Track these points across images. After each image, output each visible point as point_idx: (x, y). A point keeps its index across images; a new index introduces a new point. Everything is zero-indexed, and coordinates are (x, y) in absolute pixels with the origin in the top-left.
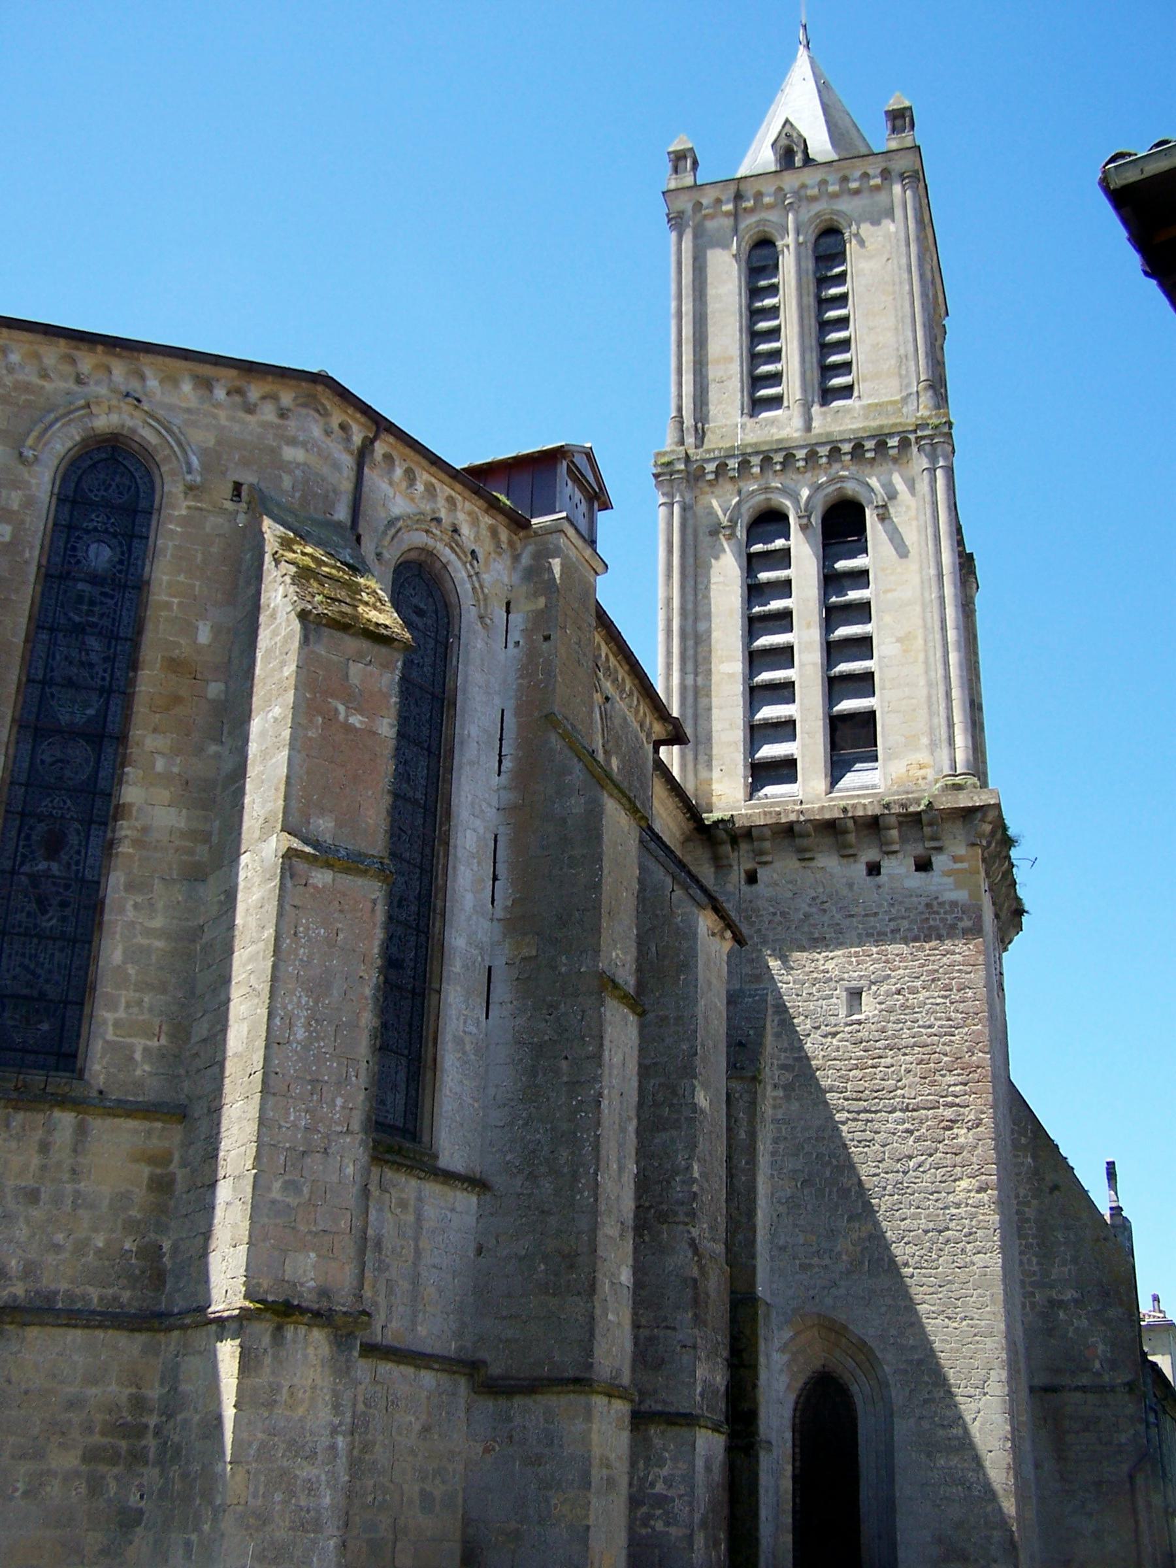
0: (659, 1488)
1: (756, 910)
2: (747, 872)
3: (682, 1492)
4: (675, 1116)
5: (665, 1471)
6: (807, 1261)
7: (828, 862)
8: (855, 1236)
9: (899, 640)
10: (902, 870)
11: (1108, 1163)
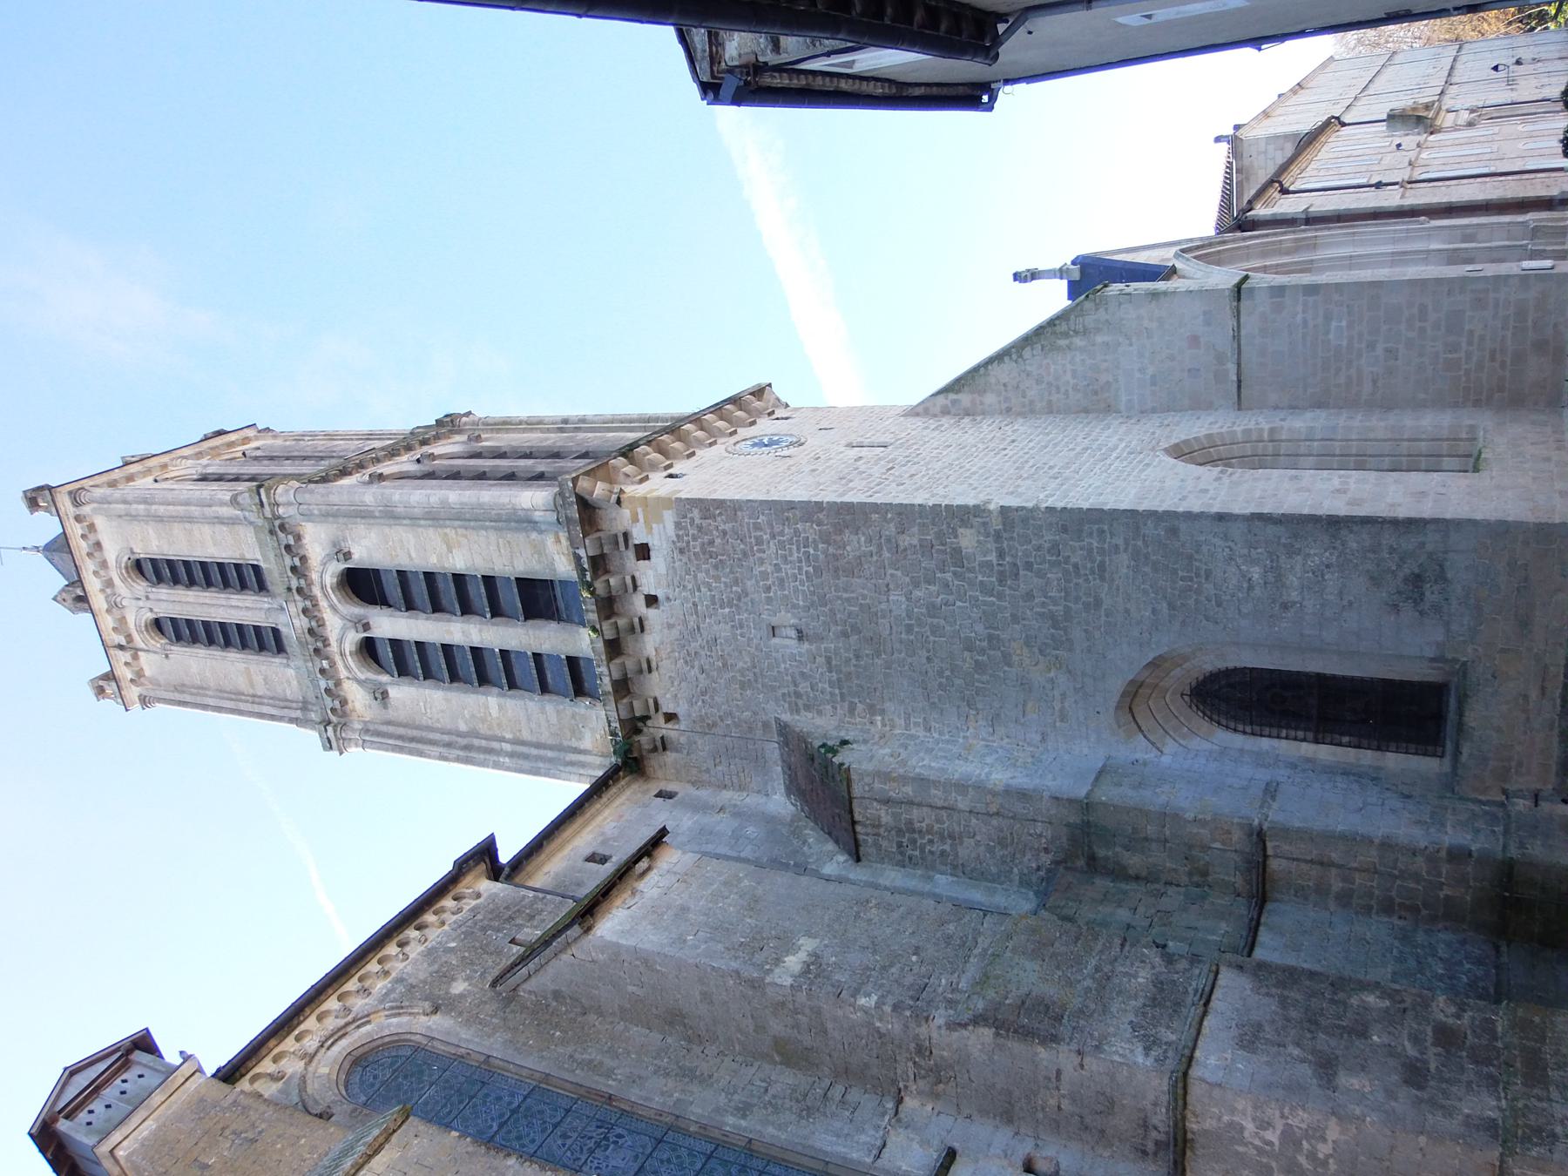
0: (1272, 1136)
3: (1277, 1113)
4: (807, 1011)
5: (1250, 1126)
6: (1057, 713)
7: (650, 644)
8: (1027, 661)
9: (450, 550)
10: (651, 573)
11: (1015, 280)
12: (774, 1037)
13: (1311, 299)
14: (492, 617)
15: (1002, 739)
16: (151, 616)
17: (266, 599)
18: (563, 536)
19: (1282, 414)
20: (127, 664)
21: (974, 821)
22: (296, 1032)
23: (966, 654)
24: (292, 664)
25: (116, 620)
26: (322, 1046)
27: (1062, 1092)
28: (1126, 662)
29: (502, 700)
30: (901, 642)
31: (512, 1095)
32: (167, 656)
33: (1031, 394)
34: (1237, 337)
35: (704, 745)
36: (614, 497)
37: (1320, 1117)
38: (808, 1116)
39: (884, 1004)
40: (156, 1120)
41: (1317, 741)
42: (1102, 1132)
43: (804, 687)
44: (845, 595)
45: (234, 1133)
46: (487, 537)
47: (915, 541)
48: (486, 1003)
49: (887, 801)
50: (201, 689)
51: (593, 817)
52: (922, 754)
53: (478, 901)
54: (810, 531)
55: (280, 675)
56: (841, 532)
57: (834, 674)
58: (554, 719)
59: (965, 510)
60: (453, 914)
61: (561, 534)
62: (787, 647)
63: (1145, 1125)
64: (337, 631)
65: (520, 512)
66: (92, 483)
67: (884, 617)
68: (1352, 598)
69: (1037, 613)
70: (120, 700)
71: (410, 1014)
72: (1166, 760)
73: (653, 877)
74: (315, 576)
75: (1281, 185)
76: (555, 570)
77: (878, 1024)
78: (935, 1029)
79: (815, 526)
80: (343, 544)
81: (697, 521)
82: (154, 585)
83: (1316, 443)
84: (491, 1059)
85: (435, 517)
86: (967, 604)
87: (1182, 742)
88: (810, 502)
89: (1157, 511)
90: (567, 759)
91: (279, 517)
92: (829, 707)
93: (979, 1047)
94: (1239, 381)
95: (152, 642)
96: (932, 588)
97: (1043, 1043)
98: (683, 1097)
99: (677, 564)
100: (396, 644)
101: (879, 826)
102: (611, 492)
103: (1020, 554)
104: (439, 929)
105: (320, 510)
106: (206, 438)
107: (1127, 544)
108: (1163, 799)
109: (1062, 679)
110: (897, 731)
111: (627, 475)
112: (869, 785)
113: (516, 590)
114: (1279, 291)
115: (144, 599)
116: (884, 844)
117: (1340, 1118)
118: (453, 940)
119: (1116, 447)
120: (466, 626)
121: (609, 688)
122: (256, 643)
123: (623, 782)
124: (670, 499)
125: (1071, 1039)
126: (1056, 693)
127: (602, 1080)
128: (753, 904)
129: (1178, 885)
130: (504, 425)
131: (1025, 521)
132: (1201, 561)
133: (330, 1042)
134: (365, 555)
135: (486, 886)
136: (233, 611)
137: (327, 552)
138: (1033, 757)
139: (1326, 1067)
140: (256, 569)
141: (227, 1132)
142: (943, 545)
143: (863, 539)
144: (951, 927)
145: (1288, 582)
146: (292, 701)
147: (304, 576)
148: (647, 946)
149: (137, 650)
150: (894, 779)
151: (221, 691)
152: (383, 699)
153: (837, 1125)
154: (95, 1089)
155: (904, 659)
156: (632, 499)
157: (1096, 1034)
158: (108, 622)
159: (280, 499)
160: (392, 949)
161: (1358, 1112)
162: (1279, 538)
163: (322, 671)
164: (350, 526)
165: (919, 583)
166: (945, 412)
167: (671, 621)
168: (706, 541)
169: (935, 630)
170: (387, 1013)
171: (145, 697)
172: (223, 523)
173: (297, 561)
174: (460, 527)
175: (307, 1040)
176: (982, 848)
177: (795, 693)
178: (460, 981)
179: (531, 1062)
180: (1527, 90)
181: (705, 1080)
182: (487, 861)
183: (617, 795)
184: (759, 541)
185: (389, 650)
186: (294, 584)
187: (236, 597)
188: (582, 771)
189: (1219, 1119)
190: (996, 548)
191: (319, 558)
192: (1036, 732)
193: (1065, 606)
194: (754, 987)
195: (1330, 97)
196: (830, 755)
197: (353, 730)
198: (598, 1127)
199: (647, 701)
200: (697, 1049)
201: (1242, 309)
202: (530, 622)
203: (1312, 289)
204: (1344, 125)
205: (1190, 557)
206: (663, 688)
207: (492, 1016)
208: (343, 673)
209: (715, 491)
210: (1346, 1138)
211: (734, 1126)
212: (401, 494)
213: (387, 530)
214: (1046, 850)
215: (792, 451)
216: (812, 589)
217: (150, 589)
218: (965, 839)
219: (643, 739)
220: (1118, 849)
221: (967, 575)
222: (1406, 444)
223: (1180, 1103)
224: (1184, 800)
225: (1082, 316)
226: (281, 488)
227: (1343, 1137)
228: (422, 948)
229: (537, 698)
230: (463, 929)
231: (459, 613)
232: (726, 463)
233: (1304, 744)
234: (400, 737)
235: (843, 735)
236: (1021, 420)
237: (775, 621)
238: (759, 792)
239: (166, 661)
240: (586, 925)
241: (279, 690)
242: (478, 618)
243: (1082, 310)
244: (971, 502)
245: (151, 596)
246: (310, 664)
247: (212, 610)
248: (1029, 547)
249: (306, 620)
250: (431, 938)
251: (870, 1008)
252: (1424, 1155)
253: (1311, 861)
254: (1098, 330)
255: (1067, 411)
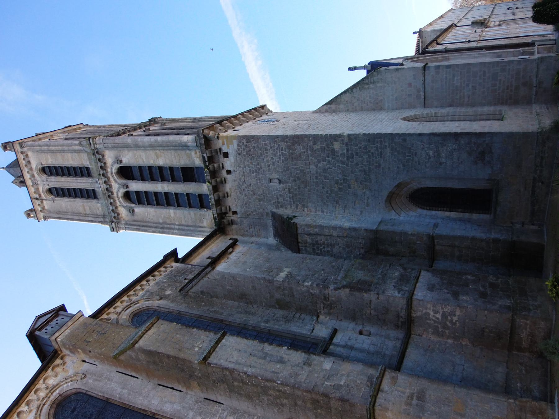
0: (439, 316)
1: (245, 213)
2: (233, 214)
3: (440, 307)
4: (288, 289)
5: (432, 313)
6: (366, 204)
7: (228, 187)
9: (158, 158)
10: (228, 162)
11: (349, 70)
12: (277, 299)
13: (448, 70)
14: (172, 181)
15: (347, 214)
16: (48, 187)
17: (91, 179)
18: (198, 151)
19: (439, 109)
20: (39, 205)
21: (339, 239)
22: (114, 306)
23: (336, 185)
24: (100, 202)
25: (35, 189)
26: (123, 310)
27: (372, 308)
28: (389, 185)
29: (175, 211)
30: (314, 182)
31: (189, 322)
32: (54, 201)
33: (355, 104)
34: (424, 83)
35: (246, 222)
36: (216, 136)
37: (453, 308)
38: (288, 322)
39: (313, 284)
40: (70, 329)
41: (450, 211)
42: (385, 320)
43: (281, 200)
44: (295, 167)
45: (97, 332)
46: (171, 153)
47: (319, 147)
48: (178, 296)
49: (309, 234)
50: (66, 213)
51: (208, 246)
52: (321, 219)
53: (172, 269)
54: (284, 145)
55: (95, 206)
56: (294, 145)
57: (291, 194)
58: (193, 216)
59: (336, 136)
60: (164, 272)
61: (197, 151)
62: (274, 186)
63: (398, 316)
64: (116, 189)
65: (183, 143)
66: (26, 141)
67: (308, 174)
68: (462, 160)
69: (360, 170)
70: (36, 218)
71: (153, 300)
72: (401, 218)
73: (234, 254)
74: (109, 170)
75: (437, 42)
76: (195, 164)
77: (311, 291)
78: (330, 291)
79: (285, 143)
80: (119, 158)
81: (245, 143)
82: (49, 176)
83: (450, 117)
84: (181, 312)
85: (152, 147)
86: (336, 168)
87: (407, 213)
88: (284, 135)
89: (399, 134)
90: (198, 230)
91: (97, 149)
92: (289, 206)
93: (345, 295)
94: (425, 98)
95: (49, 197)
96: (324, 163)
97: (366, 292)
98: (247, 319)
99: (238, 158)
100: (137, 193)
101: (307, 243)
102: (215, 134)
103: (354, 150)
104: (160, 276)
105: (112, 145)
106: (65, 128)
107: (389, 145)
108: (401, 229)
109: (368, 192)
110: (312, 213)
111: (220, 130)
112: (303, 229)
113: (181, 171)
114: (438, 67)
115: (46, 181)
116: (308, 249)
117: (460, 307)
118: (165, 279)
119: (385, 118)
120: (163, 185)
121: (214, 203)
122: (86, 195)
123: (218, 236)
124: (236, 136)
125: (375, 290)
126: (366, 197)
127: (219, 316)
128: (268, 260)
129: (406, 257)
130: (173, 120)
131: (356, 138)
132: (413, 150)
133: (125, 309)
134: (127, 161)
135: (174, 264)
136: (79, 184)
137: (114, 161)
138: (358, 219)
139: (455, 295)
140: (87, 168)
141: (95, 332)
142: (328, 148)
143: (301, 147)
144: (334, 264)
145: (442, 156)
146: (99, 215)
147: (105, 170)
148: (235, 272)
149: (42, 200)
150: (312, 227)
151: (73, 213)
152: (133, 212)
153: (298, 324)
154: (47, 323)
155: (315, 188)
156: (223, 137)
157: (382, 289)
158: (32, 190)
159: (97, 142)
160: (144, 282)
161: (466, 305)
162: (439, 141)
163: (111, 203)
164: (122, 151)
165: (320, 161)
166: (327, 111)
167: (235, 179)
168: (248, 150)
169: (326, 177)
170: (144, 300)
171: (45, 216)
172: (76, 152)
173: (103, 164)
174: (162, 150)
175: (117, 309)
176: (341, 249)
177: (278, 201)
178: (168, 291)
179: (194, 312)
180: (520, 15)
181: (254, 314)
182: (174, 257)
183: (216, 239)
184: (266, 149)
185: (135, 195)
186: (101, 172)
187: (80, 179)
188: (203, 234)
189: (422, 311)
190: (346, 148)
191: (111, 163)
192: (359, 211)
193: (369, 167)
194: (270, 282)
195: (452, 19)
196: (290, 220)
197: (122, 224)
198: (219, 330)
199: (226, 207)
200: (250, 306)
201: (426, 73)
202: (185, 183)
203: (449, 67)
204: (457, 26)
205: (410, 148)
206: (232, 203)
207: (180, 300)
208: (118, 204)
209: (251, 133)
210: (462, 314)
211: (263, 326)
212: (141, 139)
213: (135, 152)
214: (363, 248)
215: (275, 123)
216: (284, 165)
217: (48, 178)
218: (336, 246)
219: (225, 221)
220: (386, 246)
221: (336, 158)
222: (479, 116)
223: (410, 307)
224: (408, 229)
225: (373, 77)
226: (97, 138)
227: (461, 314)
228: (155, 282)
229: (188, 209)
230: (168, 276)
231: (160, 181)
232: (254, 127)
233: (446, 213)
234: (139, 226)
235: (294, 214)
236: (352, 113)
237: (271, 177)
238: (264, 237)
239: (53, 203)
240: (213, 267)
241: (95, 211)
242: (167, 182)
243: (373, 75)
244: (338, 133)
245: (48, 180)
246: (107, 201)
247: (71, 184)
248: (357, 147)
249: (106, 185)
250: (157, 279)
251: (309, 286)
252: (487, 318)
253: (449, 246)
254: (378, 82)
255: (368, 110)
